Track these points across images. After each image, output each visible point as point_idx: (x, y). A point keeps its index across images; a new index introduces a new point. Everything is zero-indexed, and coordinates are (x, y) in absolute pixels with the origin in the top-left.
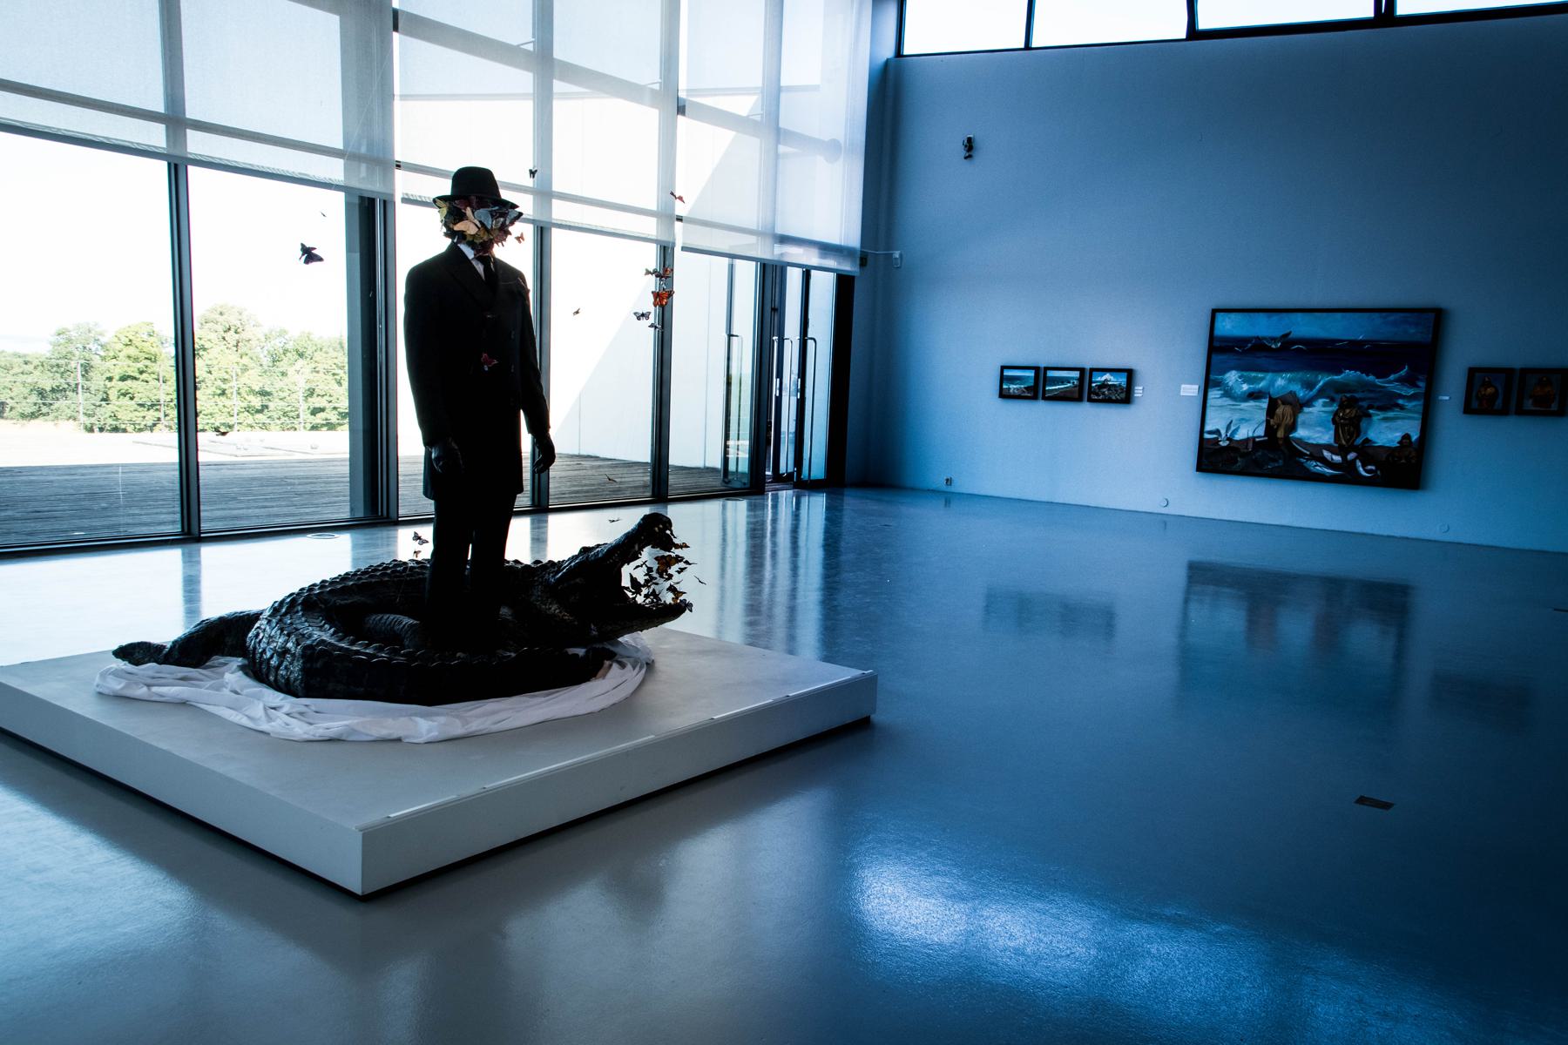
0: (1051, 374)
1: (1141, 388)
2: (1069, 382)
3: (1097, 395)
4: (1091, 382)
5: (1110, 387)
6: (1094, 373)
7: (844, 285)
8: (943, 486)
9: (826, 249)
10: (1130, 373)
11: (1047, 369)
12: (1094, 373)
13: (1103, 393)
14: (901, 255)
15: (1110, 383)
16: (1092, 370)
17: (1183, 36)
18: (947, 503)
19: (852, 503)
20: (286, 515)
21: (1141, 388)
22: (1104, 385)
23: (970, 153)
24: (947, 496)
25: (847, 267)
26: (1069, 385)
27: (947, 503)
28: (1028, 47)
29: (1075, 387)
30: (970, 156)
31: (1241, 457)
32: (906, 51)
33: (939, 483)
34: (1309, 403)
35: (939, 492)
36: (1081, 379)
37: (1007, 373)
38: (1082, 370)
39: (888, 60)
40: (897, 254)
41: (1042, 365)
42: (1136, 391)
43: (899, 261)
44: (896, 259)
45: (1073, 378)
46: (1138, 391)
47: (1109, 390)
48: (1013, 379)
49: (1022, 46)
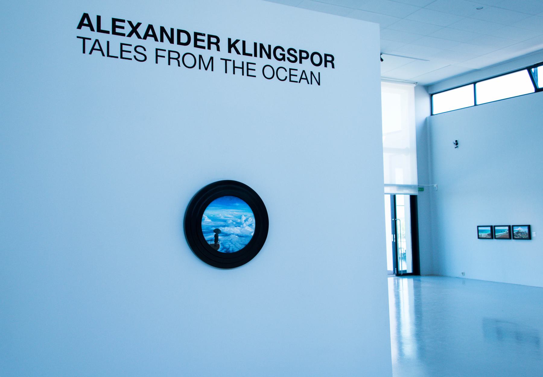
0: (496, 228)
1: (535, 233)
2: (504, 231)
3: (517, 236)
4: (513, 231)
5: (521, 233)
6: (514, 227)
7: (413, 199)
8: (461, 276)
9: (400, 187)
10: (529, 227)
11: (495, 226)
12: (514, 227)
13: (519, 236)
14: (437, 186)
15: (521, 231)
16: (513, 226)
17: (534, 91)
18: (464, 283)
19: (426, 282)
20: (397, 296)
21: (535, 233)
22: (518, 232)
23: (457, 146)
24: (464, 280)
25: (413, 193)
26: (504, 233)
27: (464, 283)
28: (475, 105)
29: (507, 233)
30: (457, 147)
31: (215, 235)
32: (434, 113)
33: (459, 274)
34: (249, 218)
35: (460, 278)
36: (509, 230)
37: (480, 228)
38: (509, 226)
39: (426, 119)
40: (435, 185)
41: (493, 225)
42: (533, 234)
43: (437, 188)
44: (435, 187)
45: (506, 230)
46: (534, 234)
47: (521, 234)
48: (483, 231)
49: (473, 105)
